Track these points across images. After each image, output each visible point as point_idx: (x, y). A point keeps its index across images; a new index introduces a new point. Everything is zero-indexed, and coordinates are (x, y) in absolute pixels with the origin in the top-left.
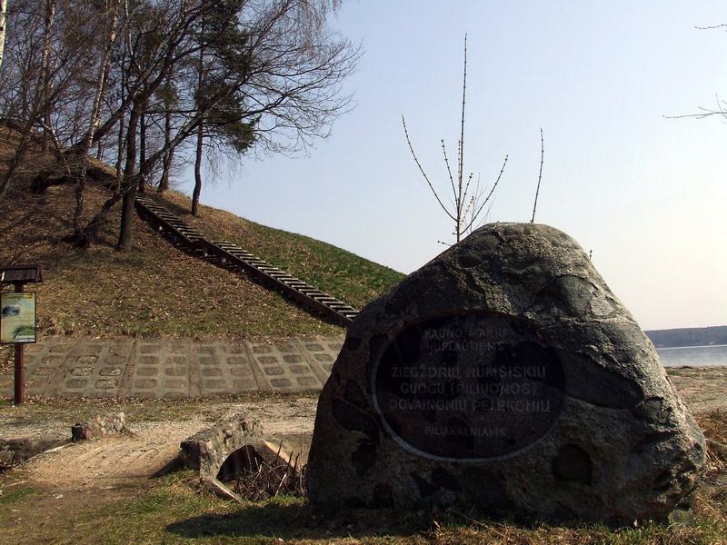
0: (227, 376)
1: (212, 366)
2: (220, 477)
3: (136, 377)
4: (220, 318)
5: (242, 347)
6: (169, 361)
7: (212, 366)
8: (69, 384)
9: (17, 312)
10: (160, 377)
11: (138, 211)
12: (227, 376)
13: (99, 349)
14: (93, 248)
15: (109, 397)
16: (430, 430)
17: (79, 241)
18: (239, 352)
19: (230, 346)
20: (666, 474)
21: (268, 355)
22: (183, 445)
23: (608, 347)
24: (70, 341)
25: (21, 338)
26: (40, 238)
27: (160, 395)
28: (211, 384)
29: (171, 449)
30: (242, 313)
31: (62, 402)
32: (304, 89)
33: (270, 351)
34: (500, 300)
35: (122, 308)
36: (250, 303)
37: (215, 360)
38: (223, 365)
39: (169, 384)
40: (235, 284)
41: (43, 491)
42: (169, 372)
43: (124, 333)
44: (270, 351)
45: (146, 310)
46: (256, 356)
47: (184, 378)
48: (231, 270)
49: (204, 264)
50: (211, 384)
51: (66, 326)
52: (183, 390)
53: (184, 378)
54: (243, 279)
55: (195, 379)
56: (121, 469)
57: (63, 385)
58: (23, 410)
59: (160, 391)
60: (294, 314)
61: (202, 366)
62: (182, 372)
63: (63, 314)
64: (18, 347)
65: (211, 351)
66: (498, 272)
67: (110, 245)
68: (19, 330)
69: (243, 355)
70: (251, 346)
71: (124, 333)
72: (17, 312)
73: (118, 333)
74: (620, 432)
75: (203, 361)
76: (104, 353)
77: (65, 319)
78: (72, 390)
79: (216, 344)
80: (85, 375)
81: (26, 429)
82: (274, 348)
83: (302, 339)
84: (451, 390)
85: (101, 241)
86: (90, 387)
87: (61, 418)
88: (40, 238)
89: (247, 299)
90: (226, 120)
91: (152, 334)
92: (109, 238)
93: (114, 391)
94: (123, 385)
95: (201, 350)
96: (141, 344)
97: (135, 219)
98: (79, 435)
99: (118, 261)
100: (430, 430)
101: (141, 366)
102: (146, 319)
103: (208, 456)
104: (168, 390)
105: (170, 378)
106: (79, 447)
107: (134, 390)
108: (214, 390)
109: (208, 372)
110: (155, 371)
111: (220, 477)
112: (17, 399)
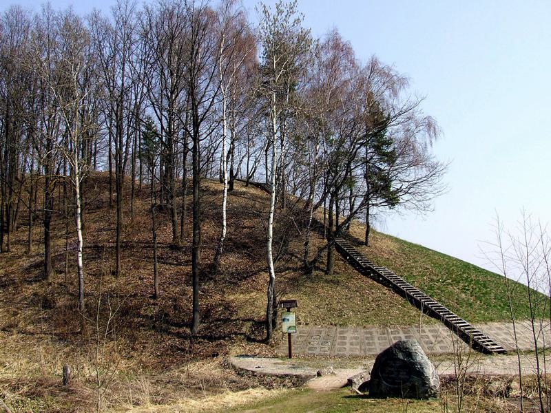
0: (377, 345)
1: (371, 341)
2: (359, 389)
3: (337, 346)
4: (376, 315)
5: (386, 332)
6: (351, 338)
7: (371, 341)
8: (310, 349)
9: (288, 320)
10: (347, 346)
11: (336, 248)
12: (377, 345)
13: (321, 332)
14: (314, 273)
15: (326, 355)
16: (389, 380)
17: (307, 269)
18: (384, 334)
19: (380, 331)
20: (427, 390)
21: (397, 335)
22: (349, 380)
23: (419, 366)
24: (308, 328)
25: (290, 331)
26: (288, 269)
27: (347, 355)
28: (370, 350)
29: (345, 381)
30: (387, 312)
31: (307, 357)
32: (420, 181)
33: (399, 333)
34: (401, 356)
35: (330, 310)
36: (392, 305)
37: (372, 338)
38: (376, 341)
39: (351, 350)
40: (385, 294)
41: (313, 390)
42: (351, 344)
43: (331, 324)
44: (399, 333)
45: (341, 311)
46: (392, 336)
47: (358, 347)
48: (384, 285)
49: (370, 281)
50: (370, 350)
51: (305, 321)
52: (358, 353)
53: (358, 347)
54: (390, 290)
55: (363, 348)
56: (333, 386)
57: (307, 350)
58: (293, 361)
59: (347, 353)
60: (414, 311)
61: (367, 341)
62: (357, 344)
63: (304, 314)
64: (289, 334)
65: (371, 333)
66: (401, 351)
67: (322, 270)
68: (289, 328)
69: (386, 336)
70: (390, 331)
71: (331, 324)
72: (288, 320)
73: (328, 324)
74: (420, 382)
75: (367, 338)
76: (323, 334)
77: (305, 317)
78: (310, 352)
79: (373, 330)
80: (316, 345)
81: (298, 370)
82: (401, 332)
83: (416, 327)
84: (392, 373)
85: (317, 268)
86: (317, 351)
87: (308, 366)
88: (288, 269)
89: (391, 303)
90: (383, 190)
91: (344, 325)
92: (322, 266)
93: (328, 353)
94: (331, 350)
95: (366, 333)
96: (339, 329)
97: (335, 253)
98: (319, 374)
99: (327, 281)
100: (389, 380)
101: (339, 341)
102: (341, 316)
103: (355, 383)
104: (351, 353)
105: (351, 346)
106: (320, 378)
107: (336, 352)
108: (371, 353)
109: (369, 344)
110: (345, 343)
111: (359, 389)
112: (290, 356)
